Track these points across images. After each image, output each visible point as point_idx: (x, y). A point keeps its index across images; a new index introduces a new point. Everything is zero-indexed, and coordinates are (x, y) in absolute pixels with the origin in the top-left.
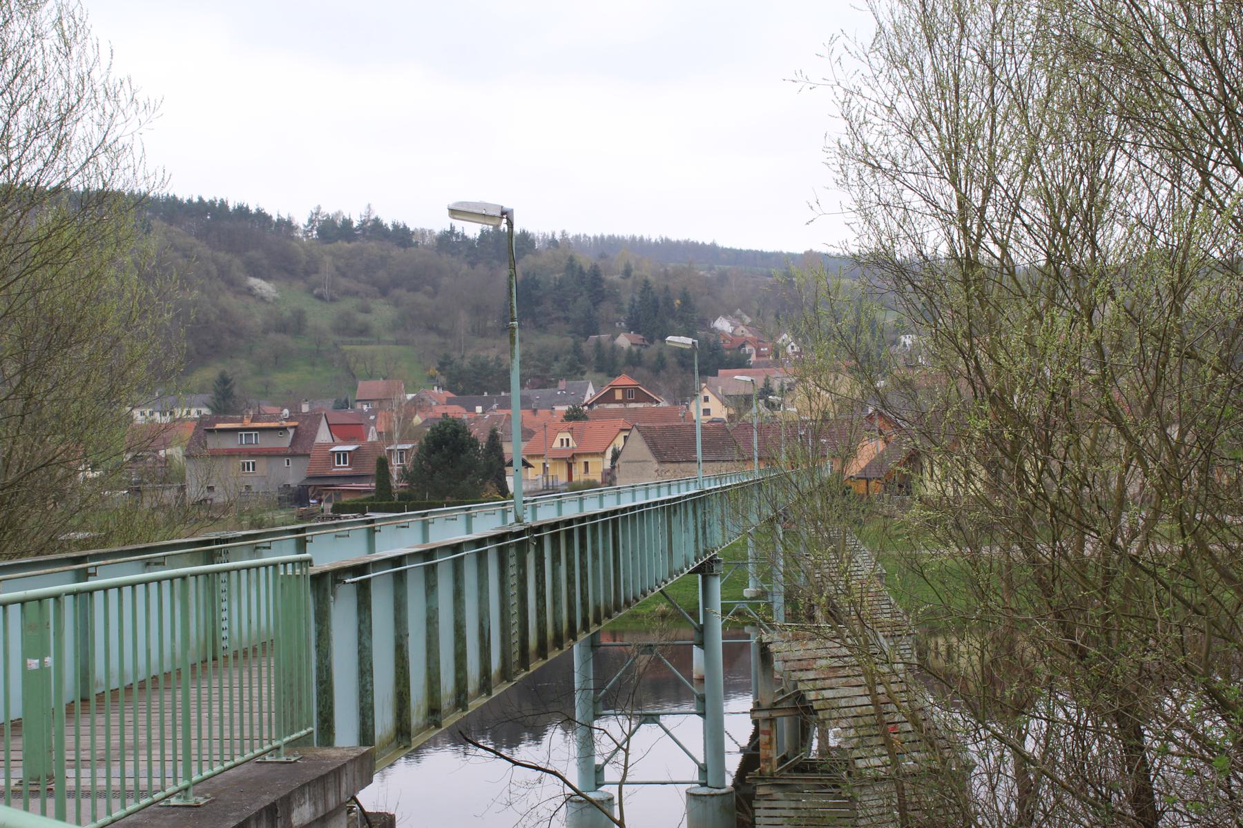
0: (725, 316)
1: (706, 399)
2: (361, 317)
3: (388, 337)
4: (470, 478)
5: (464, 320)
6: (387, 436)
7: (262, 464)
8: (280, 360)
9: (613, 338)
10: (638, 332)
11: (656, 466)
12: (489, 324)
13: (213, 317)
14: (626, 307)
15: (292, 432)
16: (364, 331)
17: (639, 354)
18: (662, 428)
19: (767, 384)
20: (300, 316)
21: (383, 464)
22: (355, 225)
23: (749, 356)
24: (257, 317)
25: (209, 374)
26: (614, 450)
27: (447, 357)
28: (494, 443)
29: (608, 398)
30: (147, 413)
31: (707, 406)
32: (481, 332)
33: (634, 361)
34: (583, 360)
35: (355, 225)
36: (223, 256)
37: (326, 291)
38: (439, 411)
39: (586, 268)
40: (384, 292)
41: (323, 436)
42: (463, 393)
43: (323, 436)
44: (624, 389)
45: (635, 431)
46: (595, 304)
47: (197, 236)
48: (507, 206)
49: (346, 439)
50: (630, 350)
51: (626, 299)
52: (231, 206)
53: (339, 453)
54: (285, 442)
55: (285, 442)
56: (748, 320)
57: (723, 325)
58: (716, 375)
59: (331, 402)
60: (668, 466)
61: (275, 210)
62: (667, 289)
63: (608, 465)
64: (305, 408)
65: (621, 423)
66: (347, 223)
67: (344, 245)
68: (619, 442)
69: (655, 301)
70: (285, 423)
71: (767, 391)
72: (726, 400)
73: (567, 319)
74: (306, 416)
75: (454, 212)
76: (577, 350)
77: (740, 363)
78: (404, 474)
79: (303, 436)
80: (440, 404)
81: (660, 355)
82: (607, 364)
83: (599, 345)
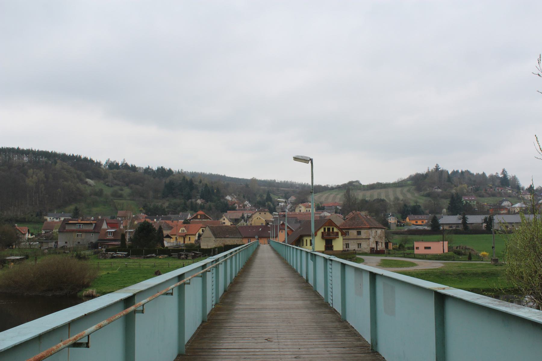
1: (224, 219)
2: (120, 192)
3: (128, 198)
6: (125, 227)
7: (84, 235)
9: (196, 201)
10: (203, 199)
12: (159, 195)
15: (94, 225)
16: (121, 196)
17: (204, 205)
19: (243, 215)
20: (101, 191)
21: (123, 236)
22: (450, 173)
24: (88, 190)
25: (72, 207)
26: (199, 234)
28: (161, 230)
29: (196, 218)
30: (52, 218)
33: (202, 208)
35: (450, 173)
36: (79, 172)
37: (110, 184)
38: (143, 220)
39: (189, 180)
40: (127, 185)
41: (105, 226)
42: (150, 215)
43: (105, 226)
44: (201, 215)
47: (71, 166)
49: (112, 228)
50: (201, 204)
52: (82, 157)
53: (109, 232)
55: (92, 228)
57: (228, 198)
59: (109, 217)
61: (96, 159)
63: (197, 238)
64: (100, 217)
65: (201, 225)
66: (117, 164)
67: (116, 170)
71: (243, 217)
72: (230, 220)
73: (182, 195)
74: (99, 220)
76: (185, 204)
77: (234, 209)
78: (130, 239)
79: (98, 227)
80: (143, 217)
81: (210, 206)
82: (194, 208)
83: (192, 202)
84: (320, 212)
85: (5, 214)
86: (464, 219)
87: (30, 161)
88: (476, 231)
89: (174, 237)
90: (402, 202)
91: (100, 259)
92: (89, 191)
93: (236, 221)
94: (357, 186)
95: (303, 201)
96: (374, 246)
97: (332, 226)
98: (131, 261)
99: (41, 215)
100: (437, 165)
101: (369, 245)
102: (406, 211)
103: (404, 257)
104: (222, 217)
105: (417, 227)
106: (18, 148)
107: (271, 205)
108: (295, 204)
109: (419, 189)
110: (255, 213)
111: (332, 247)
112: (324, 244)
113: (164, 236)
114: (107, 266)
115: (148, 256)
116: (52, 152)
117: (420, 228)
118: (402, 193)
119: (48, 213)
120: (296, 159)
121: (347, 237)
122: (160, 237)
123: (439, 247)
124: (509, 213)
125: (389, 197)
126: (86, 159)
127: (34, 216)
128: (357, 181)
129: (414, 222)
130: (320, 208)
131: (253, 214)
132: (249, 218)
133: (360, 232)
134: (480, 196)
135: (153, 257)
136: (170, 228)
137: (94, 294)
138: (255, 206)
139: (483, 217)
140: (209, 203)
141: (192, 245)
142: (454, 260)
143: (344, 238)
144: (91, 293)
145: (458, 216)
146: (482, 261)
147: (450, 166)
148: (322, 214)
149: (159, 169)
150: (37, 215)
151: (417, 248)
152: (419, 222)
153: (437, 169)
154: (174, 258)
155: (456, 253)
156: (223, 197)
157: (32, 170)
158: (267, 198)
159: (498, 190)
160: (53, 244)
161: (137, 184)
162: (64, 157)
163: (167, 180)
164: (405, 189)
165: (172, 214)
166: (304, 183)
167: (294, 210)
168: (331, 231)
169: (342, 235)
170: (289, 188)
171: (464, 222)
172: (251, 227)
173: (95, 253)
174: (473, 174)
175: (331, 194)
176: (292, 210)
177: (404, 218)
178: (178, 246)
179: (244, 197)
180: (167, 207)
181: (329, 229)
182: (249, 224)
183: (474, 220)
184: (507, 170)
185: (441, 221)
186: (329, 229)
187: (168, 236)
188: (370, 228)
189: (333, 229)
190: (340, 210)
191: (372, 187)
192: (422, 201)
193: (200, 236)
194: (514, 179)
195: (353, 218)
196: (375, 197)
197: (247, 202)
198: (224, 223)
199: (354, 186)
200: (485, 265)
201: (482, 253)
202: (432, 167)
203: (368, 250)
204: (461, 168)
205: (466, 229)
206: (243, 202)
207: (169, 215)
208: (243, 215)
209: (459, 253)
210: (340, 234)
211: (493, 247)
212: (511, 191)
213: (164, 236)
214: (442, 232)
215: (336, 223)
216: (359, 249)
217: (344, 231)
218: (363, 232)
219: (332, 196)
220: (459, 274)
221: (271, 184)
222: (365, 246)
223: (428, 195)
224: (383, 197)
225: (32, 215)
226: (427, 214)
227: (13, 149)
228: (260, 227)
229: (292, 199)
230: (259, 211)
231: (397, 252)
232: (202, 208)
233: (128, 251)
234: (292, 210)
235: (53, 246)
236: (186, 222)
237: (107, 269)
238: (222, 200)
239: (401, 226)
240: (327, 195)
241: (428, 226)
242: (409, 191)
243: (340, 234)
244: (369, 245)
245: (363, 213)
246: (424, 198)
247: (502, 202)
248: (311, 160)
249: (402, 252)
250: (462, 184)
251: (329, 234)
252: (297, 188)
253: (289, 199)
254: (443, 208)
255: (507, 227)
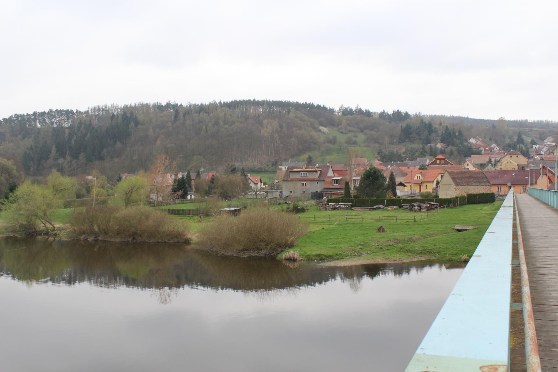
1: (468, 165)
3: (364, 145)
4: (380, 190)
5: (387, 139)
7: (309, 184)
8: (328, 152)
9: (436, 145)
11: (455, 187)
12: (395, 141)
13: (308, 138)
14: (440, 135)
15: (319, 172)
16: (355, 143)
17: (444, 150)
19: (490, 160)
20: (335, 138)
21: (347, 184)
22: (353, 110)
24: (322, 139)
25: (306, 156)
27: (380, 150)
28: (392, 178)
29: (434, 163)
31: (468, 167)
32: (392, 143)
33: (442, 152)
34: (425, 152)
35: (353, 110)
39: (427, 123)
40: (362, 131)
41: (330, 174)
43: (330, 174)
44: (440, 160)
45: (446, 173)
46: (430, 134)
47: (305, 114)
50: (441, 149)
51: (440, 133)
54: (316, 176)
55: (316, 176)
56: (481, 140)
57: (472, 141)
60: (460, 187)
61: (328, 106)
62: (454, 129)
63: (435, 186)
65: (440, 171)
66: (351, 110)
67: (350, 116)
68: (439, 178)
69: (450, 133)
70: (317, 169)
71: (490, 162)
72: (475, 165)
73: (420, 139)
76: (423, 148)
77: (479, 153)
79: (323, 174)
81: (451, 150)
82: (433, 153)
83: (431, 147)
85: (244, 165)
87: (264, 112)
89: (408, 185)
91: (320, 210)
92: (322, 139)
93: (482, 166)
98: (354, 213)
99: (276, 164)
106: (254, 100)
107: (524, 148)
110: (505, 156)
113: (397, 183)
114: (325, 220)
115: (375, 207)
116: (285, 101)
119: (283, 163)
122: (393, 186)
126: (319, 107)
127: (270, 166)
131: (501, 158)
132: (497, 162)
135: (380, 208)
136: (404, 174)
137: (295, 257)
138: (503, 149)
141: (428, 194)
144: (291, 255)
149: (394, 113)
150: (273, 165)
154: (404, 209)
156: (466, 140)
157: (266, 120)
158: (518, 140)
160: (278, 193)
161: (372, 130)
162: (297, 106)
163: (404, 124)
165: (409, 160)
172: (502, 172)
173: (318, 204)
178: (413, 195)
179: (490, 139)
180: (404, 153)
182: (498, 169)
187: (401, 184)
193: (438, 183)
197: (494, 145)
198: (468, 169)
207: (406, 162)
208: (490, 160)
213: (397, 183)
221: (522, 124)
225: (268, 165)
227: (250, 101)
228: (513, 171)
230: (510, 154)
232: (442, 152)
233: (352, 201)
235: (278, 196)
236: (423, 168)
237: (323, 223)
238: (465, 144)
252: (554, 127)
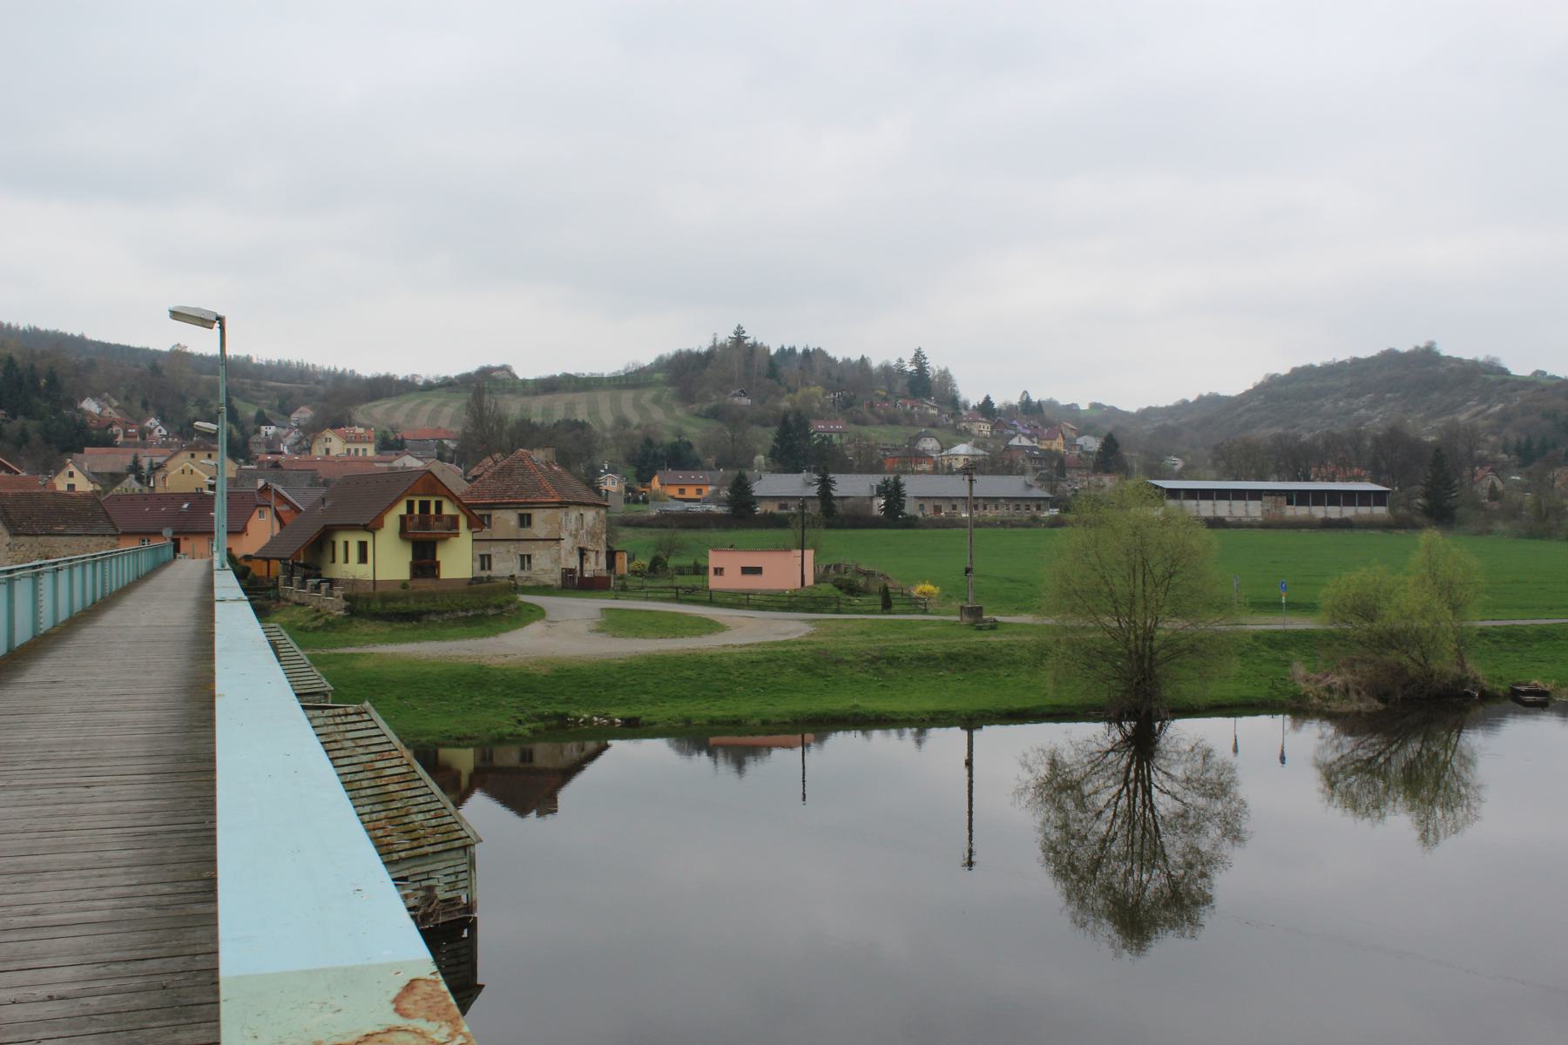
0: (93, 397)
1: (71, 475)
11: (8, 539)
18: (16, 495)
19: (136, 461)
20: (402, 518)
22: (773, 352)
23: (116, 436)
31: (71, 481)
35: (773, 352)
48: (220, 314)
56: (116, 404)
57: (90, 406)
58: (82, 452)
60: (23, 539)
62: (32, 367)
71: (135, 468)
72: (94, 477)
75: (176, 315)
77: (108, 442)
84: (390, 455)
86: (826, 485)
88: (857, 519)
90: (637, 432)
94: (503, 382)
95: (338, 423)
96: (573, 562)
97: (435, 495)
100: (739, 327)
101: (557, 560)
102: (650, 458)
103: (678, 600)
104: (66, 465)
105: (687, 505)
108: (311, 431)
109: (686, 397)
111: (436, 566)
112: (410, 559)
117: (697, 508)
118: (637, 405)
120: (176, 315)
121: (486, 533)
123: (786, 569)
124: (936, 470)
125: (602, 414)
128: (505, 368)
129: (674, 491)
130: (390, 444)
133: (529, 516)
134: (855, 423)
139: (877, 479)
140: (21, 420)
142: (838, 612)
143: (477, 536)
145: (804, 475)
146: (925, 612)
147: (775, 334)
148: (398, 463)
151: (719, 571)
152: (691, 492)
153: (739, 338)
155: (843, 588)
156: (72, 403)
159: (904, 405)
164: (647, 395)
166: (340, 370)
167: (309, 449)
168: (433, 511)
169: (470, 527)
170: (293, 382)
171: (825, 495)
174: (834, 361)
175: (425, 402)
176: (303, 447)
177: (645, 478)
179: (145, 405)
181: (425, 506)
183: (850, 486)
184: (926, 352)
185: (759, 489)
186: (425, 506)
188: (562, 505)
189: (439, 505)
190: (454, 452)
191: (549, 386)
192: (696, 431)
194: (945, 377)
195: (506, 471)
196: (559, 414)
197: (152, 422)
199: (495, 380)
200: (938, 626)
201: (920, 588)
202: (725, 335)
203: (554, 578)
204: (800, 342)
205: (834, 513)
206: (141, 420)
208: (136, 461)
209: (851, 589)
210: (463, 522)
211: (968, 571)
212: (935, 412)
214: (911, 523)
215: (454, 490)
216: (525, 574)
217: (477, 512)
218: (538, 516)
219: (428, 408)
220: (874, 661)
222: (546, 566)
223: (715, 414)
224: (581, 415)
226: (710, 469)
228: (185, 497)
229: (304, 414)
231: (648, 583)
234: (303, 447)
239: (636, 501)
240: (412, 404)
241: (718, 502)
242: (656, 401)
243: (463, 522)
244: (557, 560)
245: (539, 455)
246: (702, 422)
247: (918, 438)
248: (221, 320)
249: (666, 583)
250: (807, 384)
251: (424, 522)
252: (318, 382)
253: (294, 416)
254: (755, 454)
255: (937, 509)
